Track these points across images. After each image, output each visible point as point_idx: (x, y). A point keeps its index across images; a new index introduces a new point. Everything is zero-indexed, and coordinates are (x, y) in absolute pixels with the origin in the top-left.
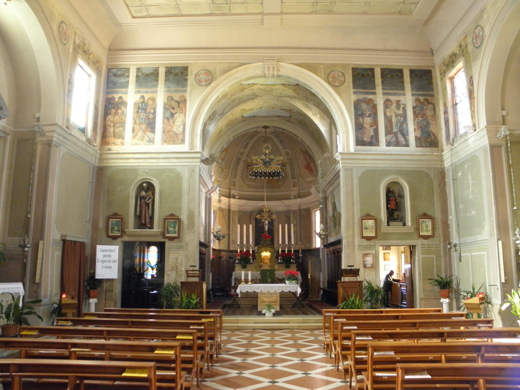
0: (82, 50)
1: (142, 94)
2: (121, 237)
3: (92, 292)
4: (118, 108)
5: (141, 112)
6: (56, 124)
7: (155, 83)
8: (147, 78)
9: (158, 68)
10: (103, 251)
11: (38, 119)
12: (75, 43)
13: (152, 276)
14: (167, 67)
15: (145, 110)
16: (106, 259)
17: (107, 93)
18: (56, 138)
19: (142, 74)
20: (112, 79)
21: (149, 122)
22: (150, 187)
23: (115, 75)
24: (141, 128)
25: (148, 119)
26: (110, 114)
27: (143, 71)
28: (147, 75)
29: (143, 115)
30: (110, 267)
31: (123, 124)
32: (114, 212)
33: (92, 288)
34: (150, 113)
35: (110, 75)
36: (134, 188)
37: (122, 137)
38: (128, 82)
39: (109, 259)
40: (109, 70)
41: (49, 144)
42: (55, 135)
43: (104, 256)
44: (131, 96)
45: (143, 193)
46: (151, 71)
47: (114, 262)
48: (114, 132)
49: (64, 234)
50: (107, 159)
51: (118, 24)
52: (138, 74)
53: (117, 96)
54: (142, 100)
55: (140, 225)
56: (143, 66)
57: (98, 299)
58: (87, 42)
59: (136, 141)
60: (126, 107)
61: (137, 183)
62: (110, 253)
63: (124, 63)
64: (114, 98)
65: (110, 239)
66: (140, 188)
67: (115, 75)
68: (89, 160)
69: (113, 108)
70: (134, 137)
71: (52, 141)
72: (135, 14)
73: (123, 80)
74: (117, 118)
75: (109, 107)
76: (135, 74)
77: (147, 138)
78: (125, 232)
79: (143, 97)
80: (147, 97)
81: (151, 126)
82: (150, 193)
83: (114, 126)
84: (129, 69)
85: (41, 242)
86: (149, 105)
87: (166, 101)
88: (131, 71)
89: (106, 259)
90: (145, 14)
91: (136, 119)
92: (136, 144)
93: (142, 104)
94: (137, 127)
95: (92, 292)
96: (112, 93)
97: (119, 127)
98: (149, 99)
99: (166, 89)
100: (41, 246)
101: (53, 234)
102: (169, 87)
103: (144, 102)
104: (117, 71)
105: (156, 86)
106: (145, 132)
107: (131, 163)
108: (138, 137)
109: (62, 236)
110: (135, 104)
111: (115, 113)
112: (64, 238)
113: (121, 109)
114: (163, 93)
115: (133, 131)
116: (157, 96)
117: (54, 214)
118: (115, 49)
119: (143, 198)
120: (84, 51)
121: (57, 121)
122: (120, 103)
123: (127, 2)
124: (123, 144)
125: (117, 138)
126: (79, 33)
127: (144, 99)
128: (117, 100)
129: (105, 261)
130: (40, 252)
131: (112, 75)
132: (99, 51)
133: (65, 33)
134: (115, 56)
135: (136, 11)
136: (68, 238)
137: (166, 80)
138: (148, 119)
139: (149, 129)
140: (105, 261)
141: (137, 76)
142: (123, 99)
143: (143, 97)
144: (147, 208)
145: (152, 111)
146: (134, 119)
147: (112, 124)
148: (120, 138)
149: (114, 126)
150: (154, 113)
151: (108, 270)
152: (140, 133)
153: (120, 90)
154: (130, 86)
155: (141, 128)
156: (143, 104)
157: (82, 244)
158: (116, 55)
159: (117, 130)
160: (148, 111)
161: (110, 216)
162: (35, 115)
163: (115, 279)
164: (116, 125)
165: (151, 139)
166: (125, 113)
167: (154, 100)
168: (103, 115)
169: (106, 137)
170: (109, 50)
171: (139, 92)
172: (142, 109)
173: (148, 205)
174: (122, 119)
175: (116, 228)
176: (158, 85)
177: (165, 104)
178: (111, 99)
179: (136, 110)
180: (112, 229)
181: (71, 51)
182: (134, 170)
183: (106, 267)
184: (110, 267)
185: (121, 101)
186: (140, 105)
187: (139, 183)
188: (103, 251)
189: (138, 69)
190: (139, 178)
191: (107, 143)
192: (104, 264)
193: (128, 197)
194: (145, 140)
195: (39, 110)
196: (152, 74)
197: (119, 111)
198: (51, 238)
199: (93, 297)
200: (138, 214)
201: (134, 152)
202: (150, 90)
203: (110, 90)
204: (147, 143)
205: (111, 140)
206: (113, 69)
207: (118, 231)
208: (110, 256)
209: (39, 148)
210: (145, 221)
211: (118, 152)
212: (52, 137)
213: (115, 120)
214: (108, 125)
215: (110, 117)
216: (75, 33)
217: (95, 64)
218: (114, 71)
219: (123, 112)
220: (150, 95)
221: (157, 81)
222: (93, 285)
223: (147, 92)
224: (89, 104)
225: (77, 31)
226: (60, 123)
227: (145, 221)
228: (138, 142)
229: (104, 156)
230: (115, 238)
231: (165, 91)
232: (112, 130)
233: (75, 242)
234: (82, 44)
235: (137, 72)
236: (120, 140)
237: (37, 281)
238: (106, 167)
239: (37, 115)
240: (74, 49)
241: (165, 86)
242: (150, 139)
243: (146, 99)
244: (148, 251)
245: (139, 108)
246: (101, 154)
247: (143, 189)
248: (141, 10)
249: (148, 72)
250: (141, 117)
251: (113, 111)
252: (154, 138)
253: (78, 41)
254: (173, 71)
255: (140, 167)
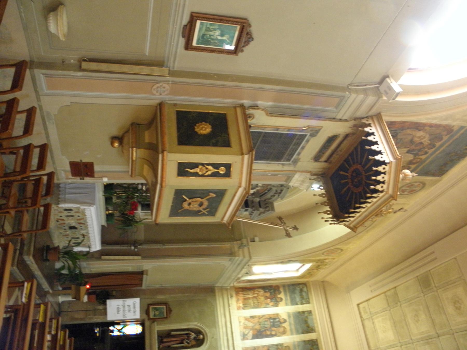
0: (319, 265)
1: (288, 320)
2: (149, 319)
3: (94, 297)
4: (271, 299)
5: (271, 322)
6: (250, 258)
7: (300, 331)
8: (304, 323)
9: (315, 332)
10: (134, 305)
11: (253, 241)
12: (325, 259)
13: (112, 331)
14: (317, 340)
15: (273, 325)
16: (127, 308)
17: (284, 286)
18: (238, 259)
19: (307, 317)
20: (297, 288)
21: (263, 331)
22: (200, 342)
23: (301, 291)
24: (255, 324)
25: (265, 330)
26: (266, 292)
27: (309, 317)
28: (306, 322)
29: (268, 324)
30: (118, 312)
31: (257, 306)
32: (172, 309)
33: (97, 296)
34: (271, 331)
35: (301, 285)
36: (197, 326)
37: (245, 306)
38: (297, 304)
39: (127, 311)
40: (305, 284)
41: (232, 254)
42: (241, 258)
43: (129, 306)
44: (284, 309)
45: (193, 335)
46: (311, 325)
47: (124, 316)
48: (248, 299)
49: (149, 273)
50: (222, 295)
51: (349, 289)
52: (306, 313)
53: (282, 295)
54: (282, 321)
55: (161, 337)
56: (314, 317)
57: (87, 302)
58: (327, 266)
59: (243, 321)
60: (274, 306)
61: (203, 329)
62: (132, 311)
63: (313, 297)
64: (280, 293)
65: (146, 308)
66: (198, 332)
67: (301, 291)
68: (220, 281)
69: (271, 294)
70: (246, 319)
71: (235, 256)
72: (361, 306)
73: (298, 299)
74: (262, 299)
75: (271, 290)
76: (305, 310)
77: (247, 332)
78: (153, 322)
79: (285, 321)
80: (286, 325)
81: (259, 334)
82: (194, 343)
83: (254, 297)
84: (308, 302)
85: (140, 257)
86: (278, 328)
87: (285, 345)
88: (308, 305)
89: (127, 308)
90: (364, 316)
91: (264, 318)
92: (240, 322)
93: (279, 321)
94: (256, 320)
95: (94, 297)
96: (285, 291)
97: (254, 303)
98: (284, 328)
99: (296, 343)
100: (136, 258)
101: (147, 265)
102: (299, 346)
103: (281, 323)
104: (305, 292)
105: (298, 333)
106: (252, 328)
107: (221, 320)
108: (247, 322)
109: (147, 271)
110: (277, 314)
111: (266, 297)
112: (145, 273)
113: (271, 302)
114: (292, 341)
115: (252, 317)
116: (288, 335)
117: (167, 264)
118: (324, 287)
119: (188, 335)
120: (319, 266)
121: (253, 258)
122: (276, 299)
123: (371, 300)
124: (239, 308)
125: (243, 302)
126: (334, 261)
127: (284, 323)
128: (279, 296)
129: (124, 307)
130: (131, 258)
131: (301, 287)
132: (320, 275)
133: (332, 253)
134: (320, 295)
135: (364, 308)
136: (145, 277)
137: (304, 341)
138: (265, 330)
139: (256, 333)
140: (124, 307)
141: (304, 312)
142: (281, 302)
143: (285, 321)
144: (178, 342)
145: (273, 333)
146: (263, 316)
147: (256, 295)
148: (244, 305)
149: (254, 297)
150: (272, 336)
151: (116, 311)
152: (250, 324)
153: (288, 298)
154: (293, 307)
155: (255, 324)
156: (278, 323)
157: (141, 285)
158: (321, 293)
159: (251, 301)
160: (273, 329)
161: (169, 305)
162: (257, 237)
163: (106, 317)
164: (255, 299)
165: (247, 337)
166: (268, 306)
167: (284, 333)
168: (263, 285)
169: (243, 291)
170: (323, 282)
171: (289, 317)
172: (274, 322)
173: (182, 343)
174: (261, 304)
175: (157, 313)
176: (299, 334)
177: (281, 345)
178: (279, 290)
179: (272, 317)
180: (156, 309)
181: (318, 258)
182: (214, 324)
183: (118, 309)
184: (118, 312)
185: (278, 300)
186: (277, 320)
187: (203, 331)
188: (134, 305)
189: (310, 312)
190: (207, 330)
191: (237, 294)
192: (121, 307)
193: (188, 320)
194: (244, 330)
195: (261, 240)
196: (308, 327)
197: (269, 300)
198: (143, 264)
199: (89, 298)
200: (173, 333)
201: (232, 321)
202: (293, 327)
203: (287, 288)
204: (242, 333)
205: (241, 297)
206: (307, 288)
207: (155, 315)
208: (129, 311)
209: (227, 245)
210: (166, 342)
211: (231, 305)
212: (239, 256)
213: (260, 297)
214: (254, 291)
215: (262, 292)
216: (334, 259)
217: (309, 273)
218: (305, 289)
219: (269, 304)
220: (288, 328)
221: (303, 333)
222: (102, 296)
223: (290, 324)
224: (272, 274)
225: (336, 260)
226: (252, 261)
227: (166, 342)
228: (242, 324)
229: (225, 292)
230: (147, 312)
231: (294, 342)
232: (251, 296)
233: (142, 280)
234: (325, 264)
235: (308, 311)
236: (241, 305)
237: (103, 257)
238: (215, 296)
239: (257, 239)
240: (319, 260)
241: (299, 342)
242: (246, 335)
243: (284, 325)
244: (137, 324)
245: (274, 319)
246: (226, 289)
247: (197, 335)
248: (367, 313)
249: (309, 322)
250: (266, 323)
251: (268, 294)
252: (247, 339)
253: (327, 261)
254: (315, 347)
255: (218, 329)
